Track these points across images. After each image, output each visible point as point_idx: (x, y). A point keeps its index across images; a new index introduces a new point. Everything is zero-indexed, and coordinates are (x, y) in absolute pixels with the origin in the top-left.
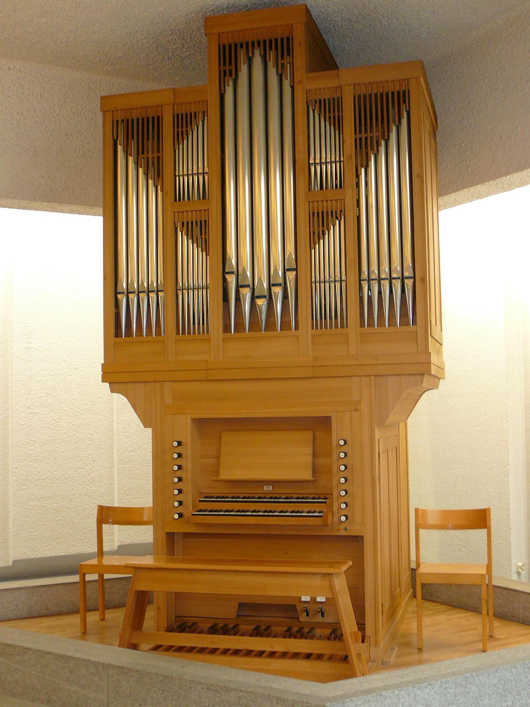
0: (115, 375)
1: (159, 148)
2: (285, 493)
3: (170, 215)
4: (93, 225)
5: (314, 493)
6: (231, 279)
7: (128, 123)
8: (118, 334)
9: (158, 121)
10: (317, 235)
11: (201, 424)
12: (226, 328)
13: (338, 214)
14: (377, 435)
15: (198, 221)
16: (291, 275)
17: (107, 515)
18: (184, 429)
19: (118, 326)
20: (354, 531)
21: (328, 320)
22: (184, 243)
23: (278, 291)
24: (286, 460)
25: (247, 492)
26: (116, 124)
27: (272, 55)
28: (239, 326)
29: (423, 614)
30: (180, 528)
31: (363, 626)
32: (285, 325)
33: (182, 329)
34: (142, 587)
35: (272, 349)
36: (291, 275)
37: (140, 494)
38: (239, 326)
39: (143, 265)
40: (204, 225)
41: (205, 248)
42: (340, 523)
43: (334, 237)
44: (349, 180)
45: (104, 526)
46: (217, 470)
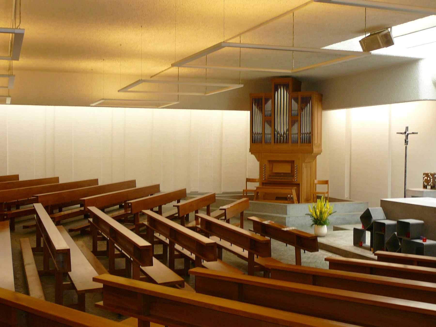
0: (252, 151)
1: (262, 105)
2: (285, 174)
3: (263, 119)
4: (248, 113)
5: (292, 174)
6: (276, 133)
7: (255, 100)
8: (253, 142)
9: (261, 99)
10: (292, 125)
11: (270, 161)
12: (275, 142)
13: (297, 121)
14: (303, 164)
15: (269, 120)
16: (287, 132)
17: (248, 180)
18: (266, 162)
19: (253, 140)
20: (298, 182)
21: (295, 142)
22: (267, 126)
23: (285, 135)
24: (286, 169)
25: (278, 174)
26: (253, 100)
27: (285, 87)
28: (277, 142)
29: (257, 184)
30: (264, 182)
31: (295, 198)
32: (286, 142)
33: (266, 142)
34: (258, 191)
35: (284, 147)
36: (287, 132)
37: (256, 176)
38: (277, 142)
39: (258, 129)
40: (271, 122)
41: (270, 126)
42: (295, 180)
43: (296, 127)
44: (299, 114)
45: (290, 172)
46: (272, 170)
